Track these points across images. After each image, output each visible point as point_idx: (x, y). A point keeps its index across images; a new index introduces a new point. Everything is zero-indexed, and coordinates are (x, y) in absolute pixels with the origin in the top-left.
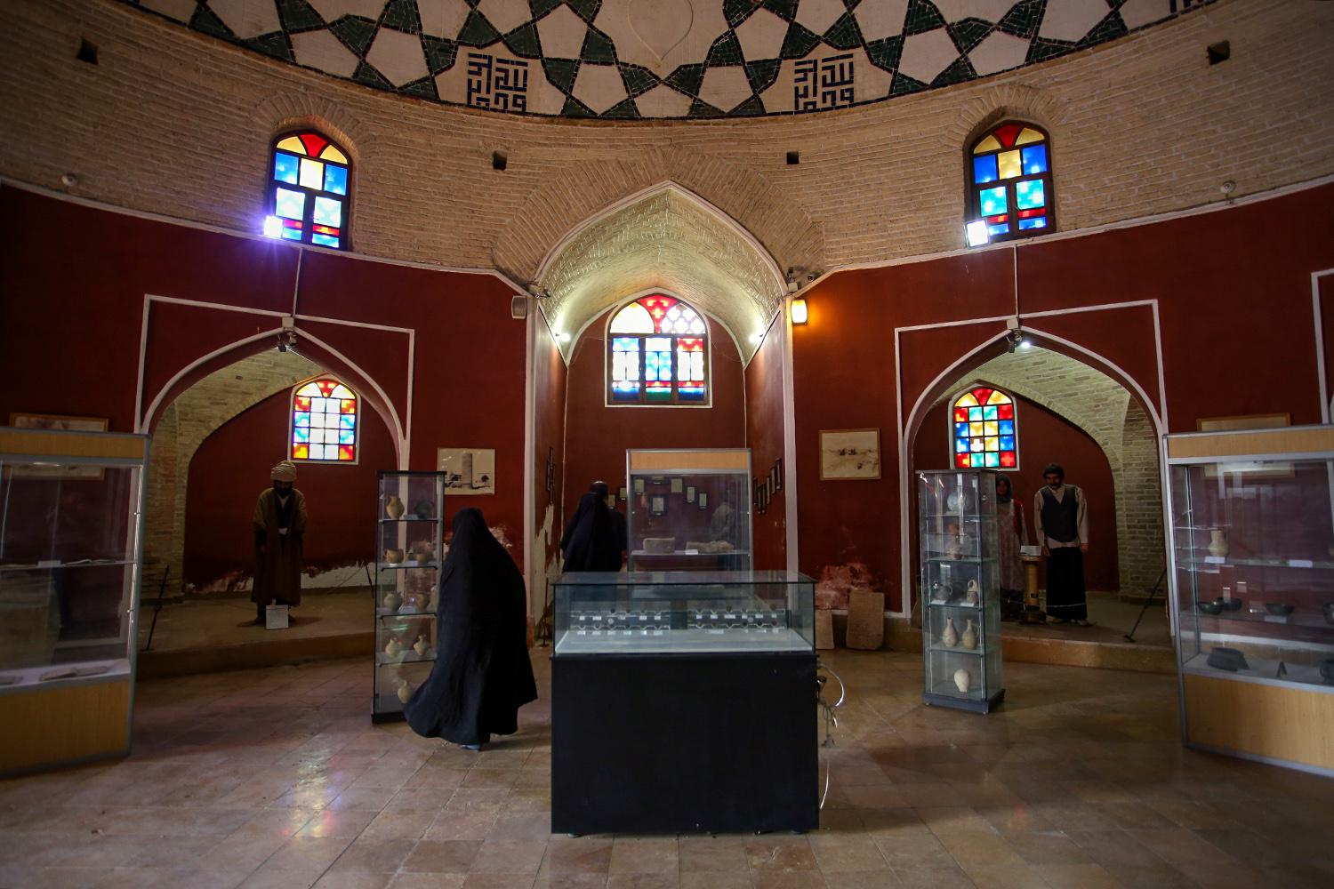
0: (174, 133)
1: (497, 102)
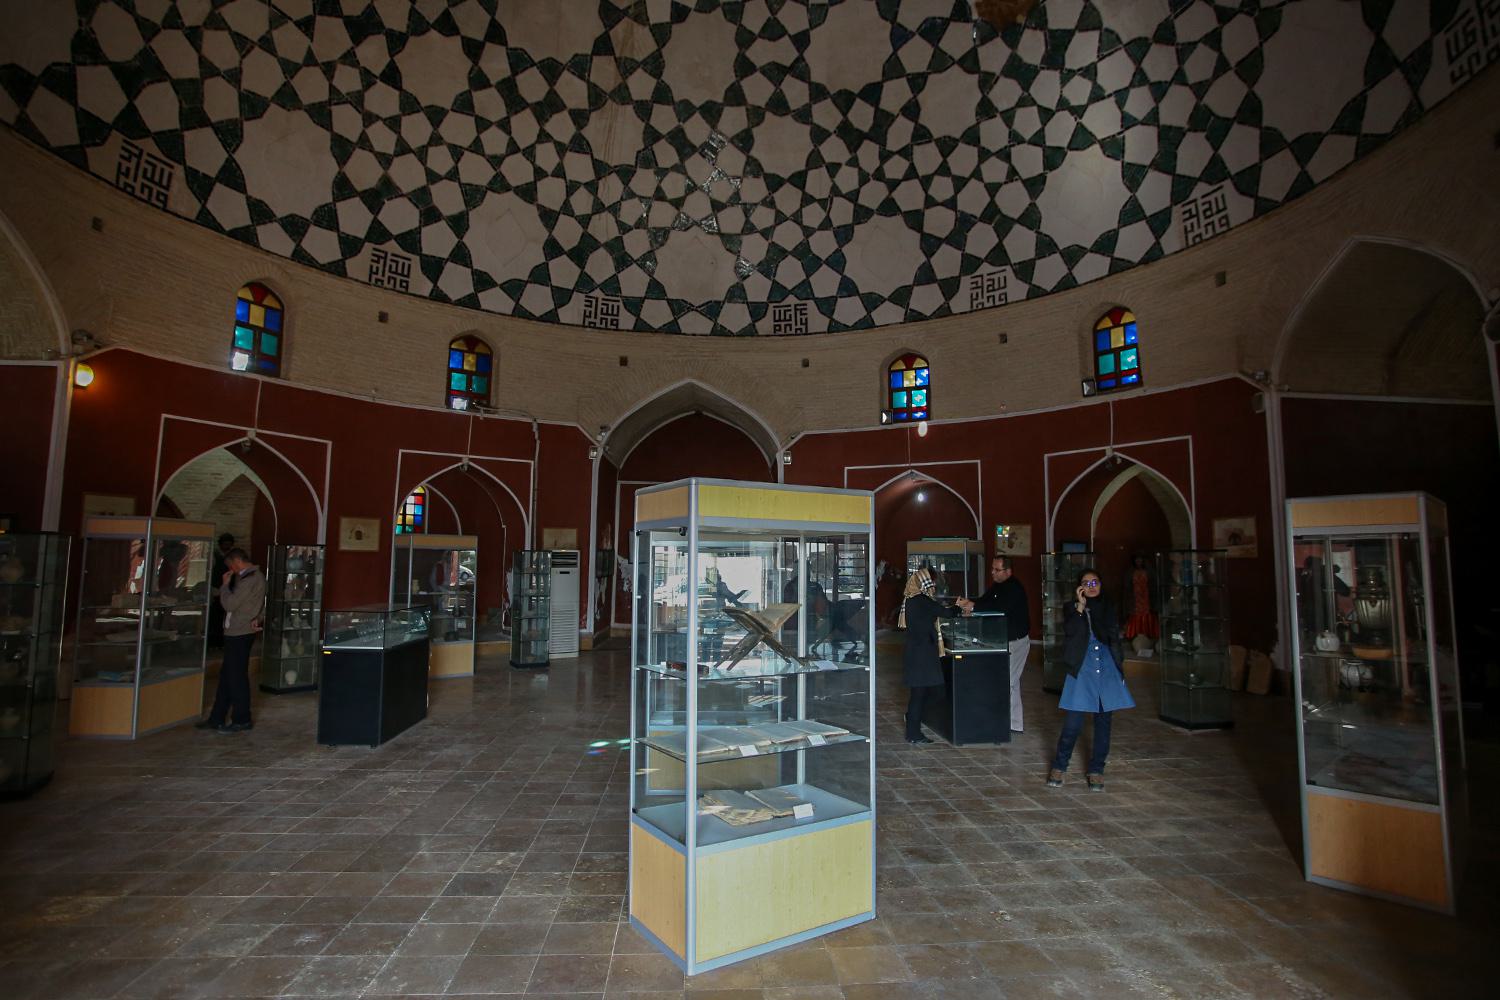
1: (389, 282)
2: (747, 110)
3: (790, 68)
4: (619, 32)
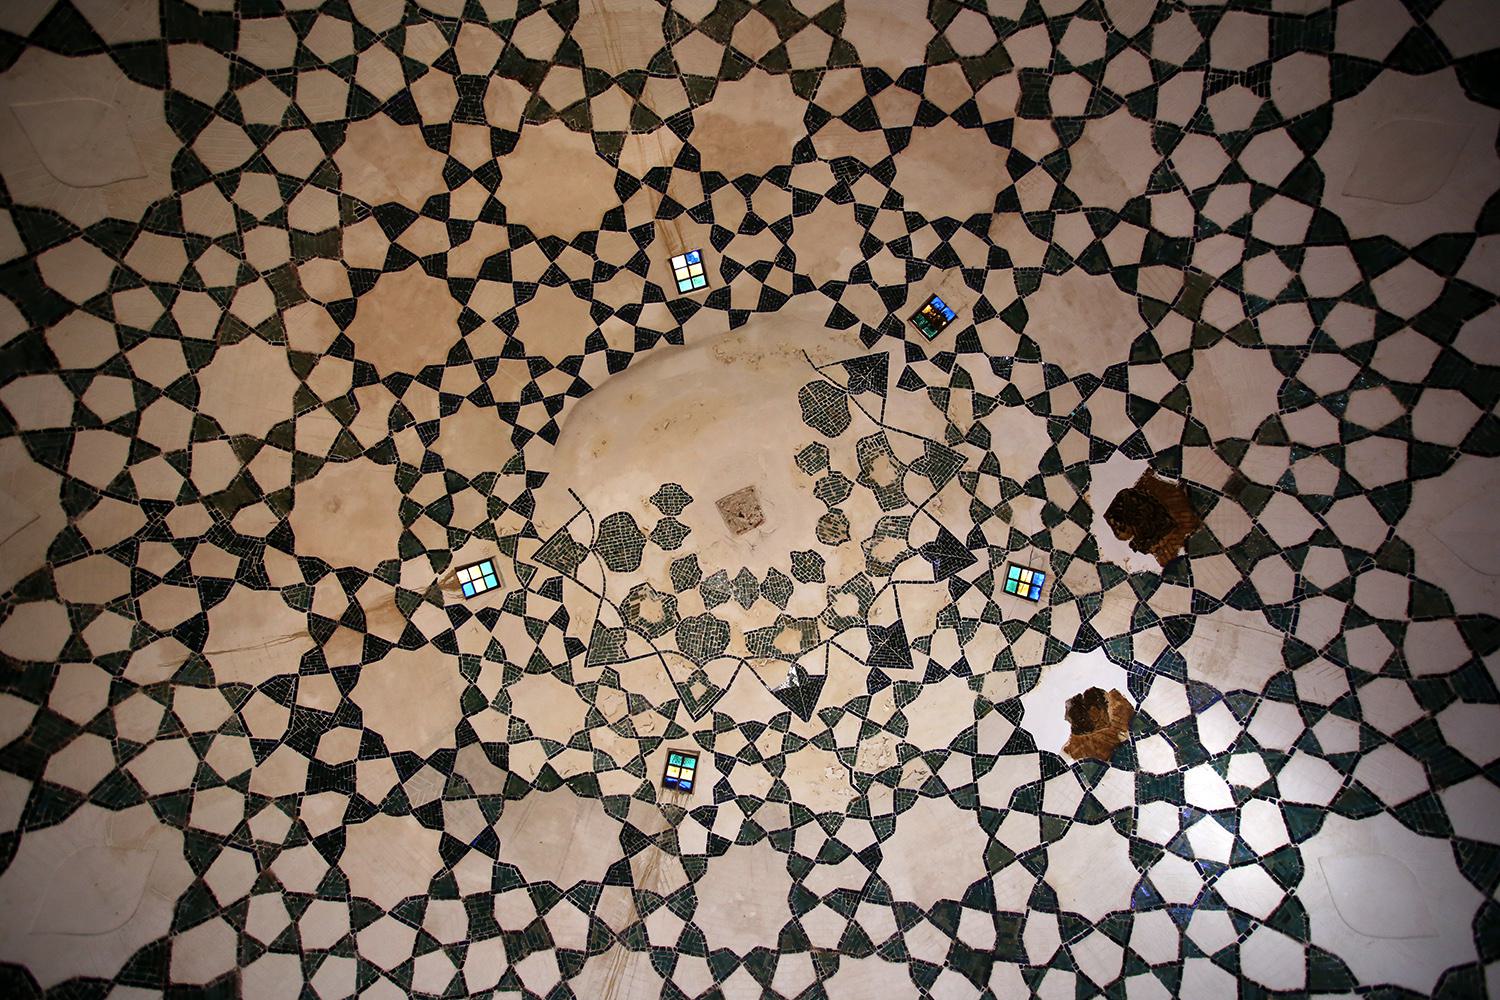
2: (812, 955)
3: (861, 893)
4: (641, 860)
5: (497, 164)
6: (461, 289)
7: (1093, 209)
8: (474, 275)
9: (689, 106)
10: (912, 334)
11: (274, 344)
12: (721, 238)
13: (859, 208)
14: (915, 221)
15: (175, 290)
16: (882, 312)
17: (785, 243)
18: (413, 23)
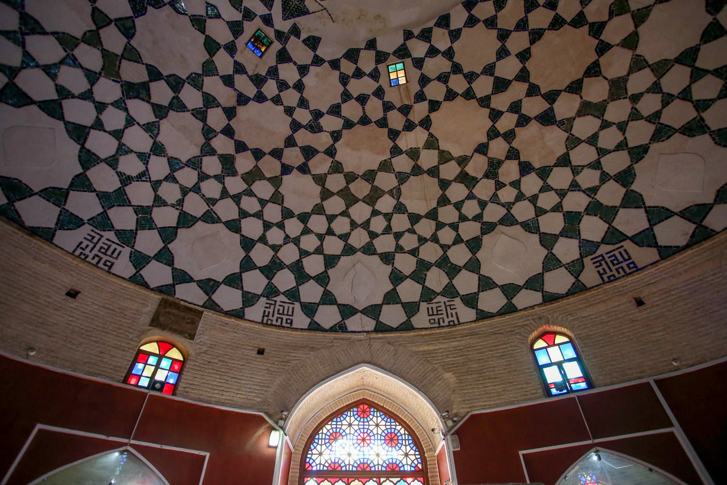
0: (698, 309)
1: (619, 273)
5: (488, 139)
6: (523, 76)
7: (184, 111)
8: (514, 83)
9: (392, 160)
10: (270, 33)
11: (641, 56)
12: (379, 93)
13: (307, 107)
14: (277, 100)
15: (680, 96)
16: (289, 47)
17: (345, 89)
18: (510, 202)
